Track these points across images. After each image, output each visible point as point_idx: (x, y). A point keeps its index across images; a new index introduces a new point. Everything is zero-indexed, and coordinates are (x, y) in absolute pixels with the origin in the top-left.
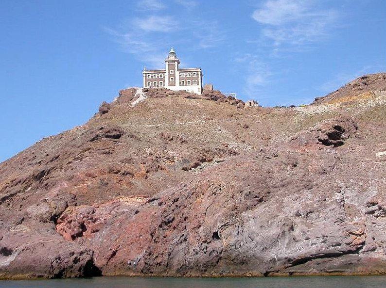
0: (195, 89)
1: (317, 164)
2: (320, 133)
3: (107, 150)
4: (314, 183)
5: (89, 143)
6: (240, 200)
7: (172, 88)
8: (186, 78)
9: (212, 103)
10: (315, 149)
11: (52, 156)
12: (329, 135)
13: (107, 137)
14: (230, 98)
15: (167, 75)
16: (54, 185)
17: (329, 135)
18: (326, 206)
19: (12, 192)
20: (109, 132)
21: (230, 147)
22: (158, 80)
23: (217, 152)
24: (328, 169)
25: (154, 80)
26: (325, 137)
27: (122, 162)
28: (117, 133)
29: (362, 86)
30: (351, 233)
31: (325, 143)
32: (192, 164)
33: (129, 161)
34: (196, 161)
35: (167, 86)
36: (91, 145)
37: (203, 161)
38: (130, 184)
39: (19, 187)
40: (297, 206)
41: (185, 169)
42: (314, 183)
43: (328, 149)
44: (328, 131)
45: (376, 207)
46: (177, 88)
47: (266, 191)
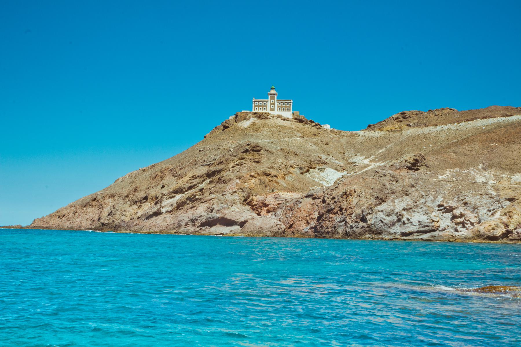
0: (288, 114)
1: (408, 181)
2: (407, 163)
3: (256, 160)
4: (410, 192)
5: (242, 154)
6: (373, 201)
7: (272, 113)
8: (282, 107)
9: (300, 125)
10: (404, 173)
11: (218, 161)
12: (411, 164)
13: (254, 151)
14: (311, 121)
15: (269, 103)
16: (229, 181)
17: (411, 164)
18: (417, 206)
19: (195, 183)
20: (254, 147)
21: (323, 158)
22: (263, 106)
23: (316, 162)
24: (415, 185)
25: (260, 106)
26: (409, 165)
27: (268, 168)
28: (258, 148)
29: (402, 119)
30: (434, 221)
31: (410, 168)
32: (305, 170)
33: (272, 168)
34: (307, 168)
35: (268, 111)
36: (245, 155)
37: (311, 168)
38: (277, 183)
39: (198, 180)
40: (404, 205)
41: (302, 173)
42: (410, 192)
43: (411, 172)
44: (412, 162)
45: (443, 208)
46: (276, 113)
47: (385, 196)
